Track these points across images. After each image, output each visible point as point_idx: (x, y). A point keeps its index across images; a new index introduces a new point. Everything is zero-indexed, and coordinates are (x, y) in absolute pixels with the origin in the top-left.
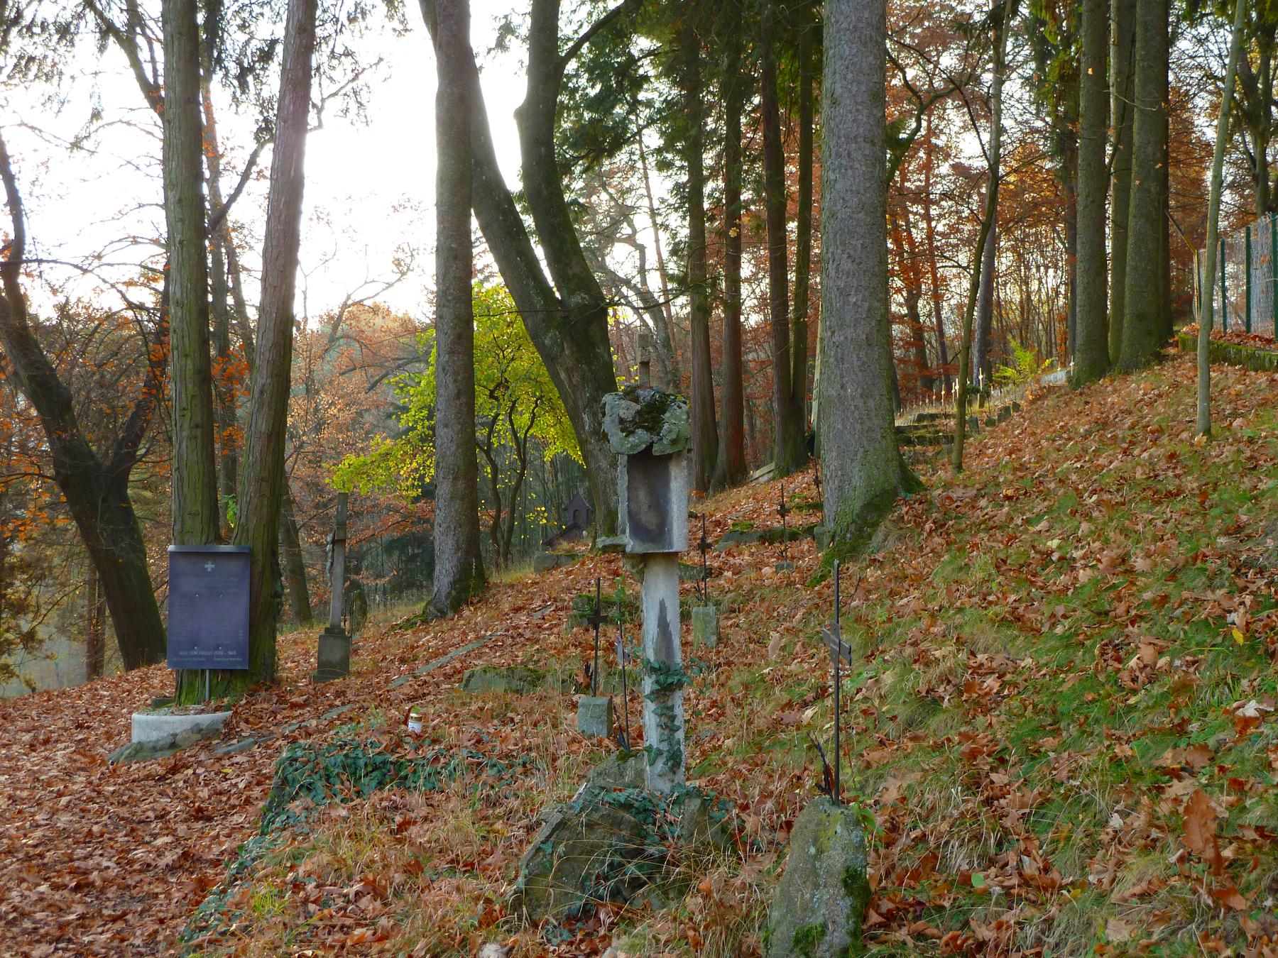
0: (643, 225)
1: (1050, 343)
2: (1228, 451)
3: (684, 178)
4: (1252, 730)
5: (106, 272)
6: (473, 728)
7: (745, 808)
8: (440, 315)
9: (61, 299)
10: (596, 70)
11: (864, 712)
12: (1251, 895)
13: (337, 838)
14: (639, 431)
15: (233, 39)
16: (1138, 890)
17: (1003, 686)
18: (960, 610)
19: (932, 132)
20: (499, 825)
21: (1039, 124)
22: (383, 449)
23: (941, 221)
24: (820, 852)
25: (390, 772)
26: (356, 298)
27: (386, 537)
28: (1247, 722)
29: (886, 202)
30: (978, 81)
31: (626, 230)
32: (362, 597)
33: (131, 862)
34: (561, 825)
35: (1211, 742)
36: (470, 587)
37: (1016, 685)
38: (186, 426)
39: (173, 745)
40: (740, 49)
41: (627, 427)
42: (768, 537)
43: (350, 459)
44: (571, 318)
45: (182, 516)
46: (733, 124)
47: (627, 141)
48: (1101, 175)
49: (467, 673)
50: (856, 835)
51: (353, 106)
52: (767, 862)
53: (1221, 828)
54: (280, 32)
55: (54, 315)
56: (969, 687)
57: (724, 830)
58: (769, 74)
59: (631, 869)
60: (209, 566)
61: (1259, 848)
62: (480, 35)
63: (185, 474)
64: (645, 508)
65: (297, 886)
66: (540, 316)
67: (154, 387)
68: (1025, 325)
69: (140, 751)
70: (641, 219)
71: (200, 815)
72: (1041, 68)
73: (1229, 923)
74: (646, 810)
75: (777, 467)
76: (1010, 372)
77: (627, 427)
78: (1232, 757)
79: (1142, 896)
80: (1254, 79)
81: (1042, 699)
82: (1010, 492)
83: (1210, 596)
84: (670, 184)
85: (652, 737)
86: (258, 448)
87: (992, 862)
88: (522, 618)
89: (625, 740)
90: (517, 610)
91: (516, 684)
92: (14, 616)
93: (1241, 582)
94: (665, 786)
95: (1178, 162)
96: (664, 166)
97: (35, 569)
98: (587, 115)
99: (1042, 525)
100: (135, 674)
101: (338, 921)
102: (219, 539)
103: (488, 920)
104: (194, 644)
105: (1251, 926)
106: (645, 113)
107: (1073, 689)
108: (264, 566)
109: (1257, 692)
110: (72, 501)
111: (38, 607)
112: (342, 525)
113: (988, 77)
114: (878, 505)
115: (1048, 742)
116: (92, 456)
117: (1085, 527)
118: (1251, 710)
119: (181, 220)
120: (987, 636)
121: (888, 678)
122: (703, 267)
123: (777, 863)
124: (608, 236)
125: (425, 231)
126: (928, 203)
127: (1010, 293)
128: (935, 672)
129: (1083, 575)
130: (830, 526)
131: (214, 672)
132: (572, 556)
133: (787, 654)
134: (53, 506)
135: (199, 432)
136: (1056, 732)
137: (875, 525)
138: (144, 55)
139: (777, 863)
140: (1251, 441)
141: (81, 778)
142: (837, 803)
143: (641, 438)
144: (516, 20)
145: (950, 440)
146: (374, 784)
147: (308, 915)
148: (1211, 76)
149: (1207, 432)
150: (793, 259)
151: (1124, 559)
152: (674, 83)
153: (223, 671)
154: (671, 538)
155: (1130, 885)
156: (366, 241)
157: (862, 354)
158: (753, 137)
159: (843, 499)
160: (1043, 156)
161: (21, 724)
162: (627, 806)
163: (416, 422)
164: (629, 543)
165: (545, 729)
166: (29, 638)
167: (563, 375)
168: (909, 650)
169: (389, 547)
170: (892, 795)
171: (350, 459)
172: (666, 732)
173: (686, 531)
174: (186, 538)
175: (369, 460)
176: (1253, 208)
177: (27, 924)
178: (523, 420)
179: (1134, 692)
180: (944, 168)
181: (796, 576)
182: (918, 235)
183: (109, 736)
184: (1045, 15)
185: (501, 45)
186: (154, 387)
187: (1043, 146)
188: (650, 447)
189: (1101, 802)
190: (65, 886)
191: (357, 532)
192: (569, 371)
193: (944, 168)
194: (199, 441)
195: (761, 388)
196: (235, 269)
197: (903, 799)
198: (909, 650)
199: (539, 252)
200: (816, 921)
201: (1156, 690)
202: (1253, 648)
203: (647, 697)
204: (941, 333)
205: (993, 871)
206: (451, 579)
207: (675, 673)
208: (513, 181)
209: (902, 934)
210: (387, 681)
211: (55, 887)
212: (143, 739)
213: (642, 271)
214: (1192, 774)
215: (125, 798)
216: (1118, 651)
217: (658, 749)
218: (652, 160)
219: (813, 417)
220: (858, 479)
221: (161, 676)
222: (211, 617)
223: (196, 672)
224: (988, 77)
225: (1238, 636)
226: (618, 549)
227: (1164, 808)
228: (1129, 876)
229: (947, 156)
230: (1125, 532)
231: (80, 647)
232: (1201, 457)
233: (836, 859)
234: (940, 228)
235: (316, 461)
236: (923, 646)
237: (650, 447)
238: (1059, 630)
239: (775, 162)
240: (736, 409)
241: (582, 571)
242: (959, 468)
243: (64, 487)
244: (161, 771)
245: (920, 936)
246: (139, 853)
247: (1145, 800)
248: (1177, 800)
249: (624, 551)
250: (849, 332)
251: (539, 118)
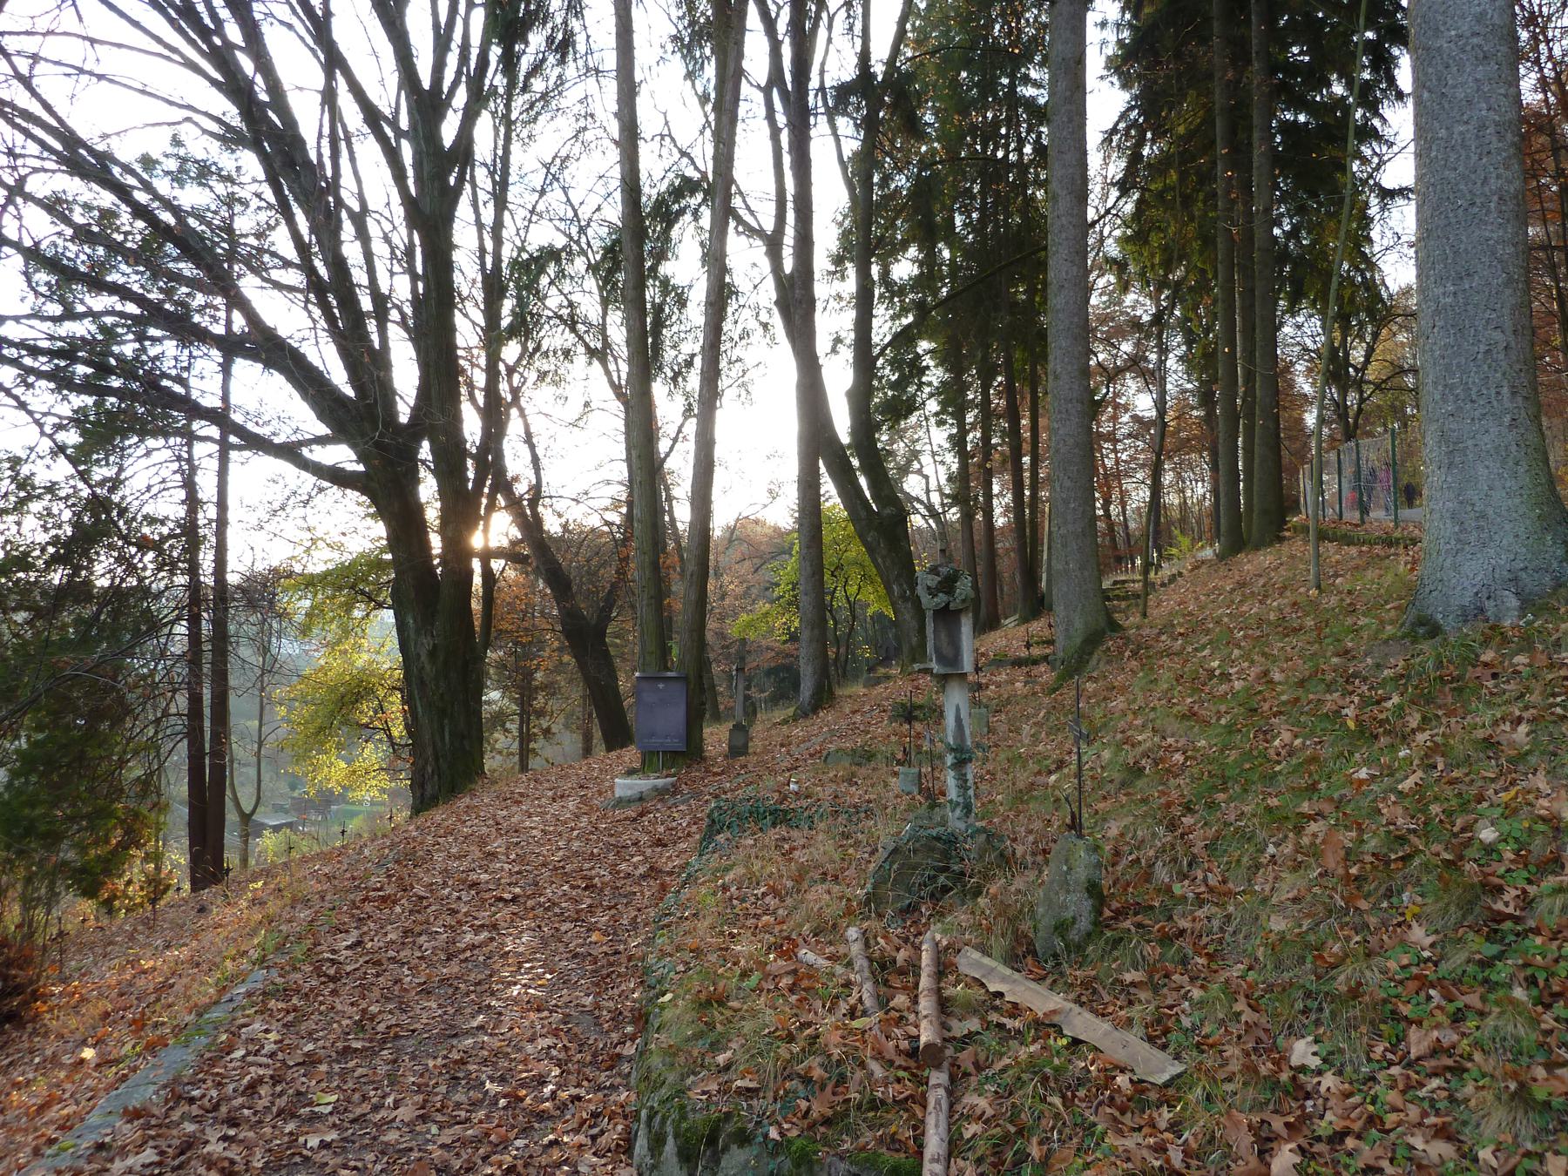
0: (928, 461)
1: (1201, 533)
2: (1334, 600)
3: (955, 431)
4: (1365, 787)
5: (591, 503)
6: (830, 789)
7: (1015, 840)
8: (799, 521)
9: (563, 520)
10: (895, 364)
11: (1092, 777)
12: (1372, 900)
13: (753, 857)
15: (669, 354)
16: (1290, 895)
17: (1186, 759)
18: (1153, 709)
19: (1117, 395)
20: (851, 851)
21: (1190, 386)
22: (764, 610)
23: (1123, 453)
24: (1070, 869)
25: (780, 817)
26: (744, 514)
27: (766, 666)
28: (1361, 782)
29: (1089, 444)
30: (1146, 359)
31: (916, 465)
32: (753, 704)
33: (618, 872)
34: (895, 851)
35: (1336, 796)
36: (823, 698)
37: (1195, 758)
39: (641, 799)
40: (989, 346)
41: (932, 592)
42: (1018, 663)
43: (744, 617)
44: (883, 521)
46: (985, 394)
47: (917, 409)
48: (1233, 418)
49: (825, 753)
50: (1094, 858)
51: (743, 393)
52: (1031, 875)
53: (1347, 854)
54: (697, 348)
55: (559, 530)
56: (1162, 760)
57: (1002, 855)
58: (1009, 362)
59: (942, 879)
60: (661, 686)
61: (1375, 868)
62: (822, 344)
65: (725, 888)
67: (621, 572)
68: (1183, 520)
70: (926, 459)
71: (659, 843)
72: (1190, 348)
73: (1357, 919)
74: (951, 841)
76: (1174, 551)
77: (932, 592)
78: (1352, 805)
79: (1295, 900)
80: (1337, 350)
81: (1214, 768)
83: (1328, 697)
84: (946, 435)
85: (953, 793)
87: (1185, 877)
88: (858, 718)
89: (933, 797)
90: (854, 712)
91: (857, 759)
93: (1350, 688)
94: (961, 825)
95: (1285, 408)
96: (940, 423)
97: (550, 689)
98: (890, 393)
99: (1206, 652)
100: (613, 754)
101: (752, 911)
102: (668, 669)
103: (849, 912)
104: (652, 735)
105: (1373, 921)
106: (927, 390)
107: (1235, 761)
109: (1367, 762)
110: (571, 646)
112: (743, 659)
113: (1153, 357)
114: (1093, 640)
115: (1221, 796)
116: (584, 618)
117: (1236, 652)
118: (1363, 774)
120: (1173, 725)
121: (1106, 754)
122: (967, 489)
123: (1038, 877)
124: (905, 470)
125: (790, 468)
126: (1115, 441)
127: (1172, 499)
128: (1139, 750)
129: (1238, 685)
130: (1061, 654)
132: (888, 678)
133: (1035, 739)
134: (560, 649)
136: (1224, 790)
137: (1091, 654)
138: (612, 367)
139: (1038, 877)
140: (1350, 592)
141: (585, 819)
142: (1081, 836)
143: (942, 598)
144: (843, 334)
145: (1138, 596)
147: (733, 907)
148: (1306, 349)
149: (1318, 587)
150: (1027, 482)
151: (1266, 673)
152: (947, 370)
155: (1285, 893)
156: (754, 476)
158: (998, 402)
159: (1068, 637)
160: (1193, 408)
161: (546, 785)
162: (938, 838)
164: (936, 667)
165: (880, 788)
166: (547, 732)
168: (1119, 736)
169: (769, 672)
170: (1114, 831)
171: (744, 617)
175: (754, 618)
176: (1339, 437)
177: (557, 910)
178: (852, 590)
179: (1279, 763)
180: (1125, 418)
181: (1038, 688)
182: (1109, 463)
183: (600, 793)
184: (1191, 315)
185: (834, 350)
186: (621, 572)
187: (1192, 401)
188: (948, 605)
189: (1262, 835)
191: (752, 663)
192: (883, 558)
193: (1125, 418)
195: (1008, 565)
196: (670, 499)
197: (1122, 835)
198: (1119, 736)
199: (863, 481)
200: (1069, 915)
201: (1294, 761)
202: (1362, 732)
204: (1127, 527)
205: (1186, 882)
207: (968, 751)
208: (845, 439)
209: (1127, 924)
210: (773, 758)
211: (573, 887)
213: (928, 492)
214: (1324, 818)
216: (1267, 734)
218: (933, 420)
219: (1043, 584)
220: (1078, 624)
221: (631, 755)
222: (662, 717)
224: (1153, 357)
225: (1351, 724)
226: (928, 671)
227: (1305, 841)
228: (1284, 886)
229: (1127, 410)
230: (1264, 654)
231: (578, 737)
232: (1314, 604)
233: (1081, 874)
234: (1124, 457)
235: (722, 619)
236: (1129, 733)
237: (948, 605)
238: (1223, 721)
239: (1014, 419)
240: (990, 578)
241: (897, 686)
242: (1145, 615)
243: (567, 637)
245: (1139, 926)
246: (623, 866)
247: (1291, 835)
248: (1315, 835)
250: (1070, 527)
251: (860, 396)
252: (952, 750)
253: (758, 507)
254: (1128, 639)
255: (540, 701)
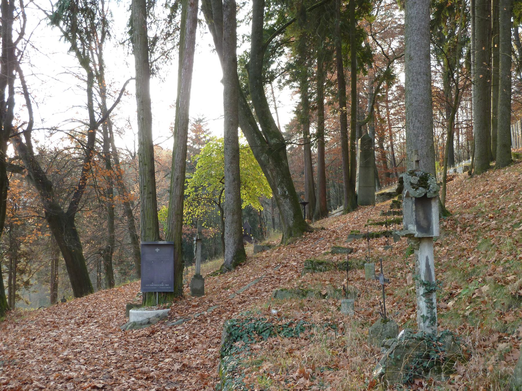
14: (421, 188)
38: (146, 193)
39: (149, 323)
45: (145, 230)
60: (157, 250)
63: (146, 213)
64: (422, 219)
66: (259, 148)
69: (135, 325)
75: (345, 209)
82: (492, 215)
86: (176, 202)
92: (21, 274)
102: (160, 239)
108: (179, 250)
111: (31, 271)
119: (143, 110)
131: (160, 293)
135: (151, 195)
143: (421, 191)
146: (268, 335)
153: (163, 292)
154: (433, 231)
157: (425, 160)
163: (190, 193)
166: (27, 284)
167: (269, 172)
172: (430, 309)
173: (438, 228)
174: (146, 239)
188: (426, 195)
190: (142, 378)
194: (151, 199)
203: (422, 295)
206: (232, 255)
207: (433, 285)
211: (138, 379)
212: (136, 320)
215: (140, 344)
217: (427, 316)
223: (152, 293)
237: (426, 195)
244: (148, 333)
249: (413, 237)
252: (424, 284)
253: (164, 138)
254: (456, 220)
255: (22, 263)
